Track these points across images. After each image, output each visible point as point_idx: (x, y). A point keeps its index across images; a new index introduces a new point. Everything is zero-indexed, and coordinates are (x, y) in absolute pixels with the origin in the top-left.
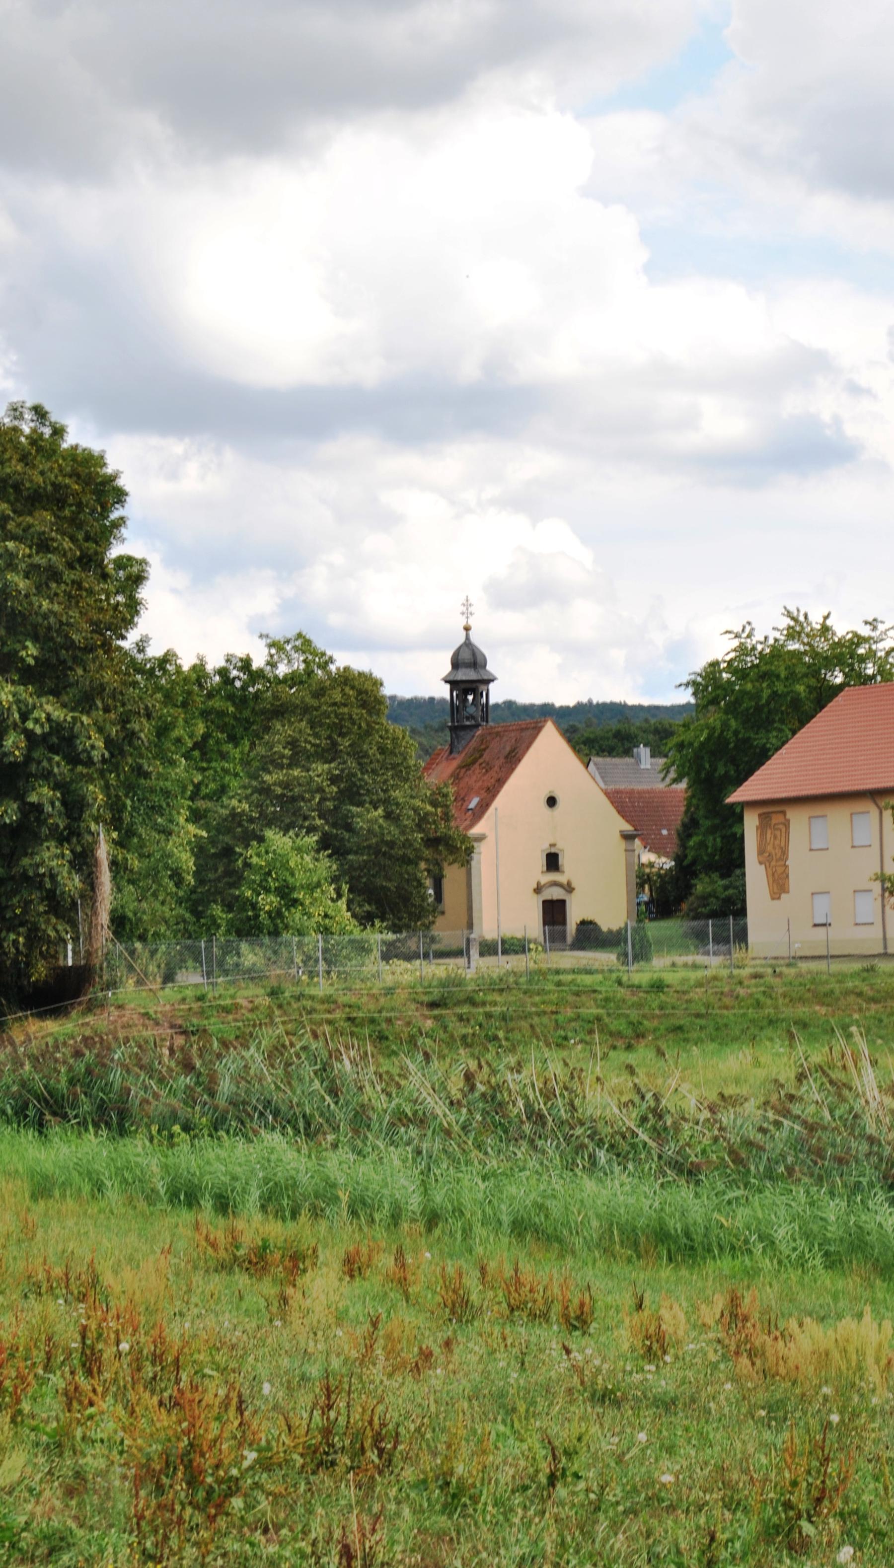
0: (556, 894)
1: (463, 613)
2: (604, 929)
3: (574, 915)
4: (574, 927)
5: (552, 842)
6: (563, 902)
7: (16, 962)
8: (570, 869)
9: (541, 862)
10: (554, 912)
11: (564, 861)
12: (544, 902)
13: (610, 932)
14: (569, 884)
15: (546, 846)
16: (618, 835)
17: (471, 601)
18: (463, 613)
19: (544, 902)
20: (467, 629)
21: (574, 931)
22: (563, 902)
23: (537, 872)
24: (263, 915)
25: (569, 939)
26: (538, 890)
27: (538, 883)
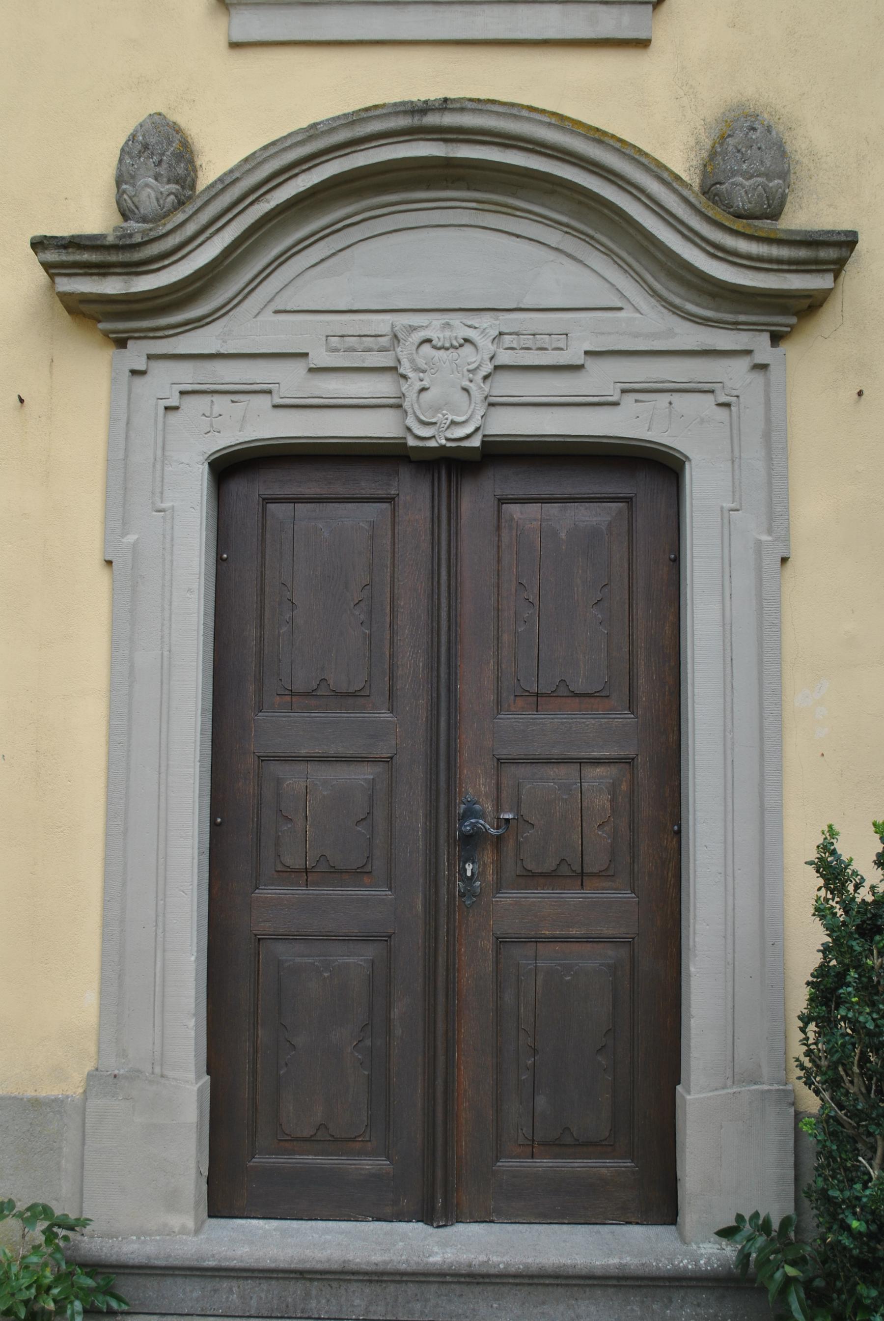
0: (444, 334)
14: (746, 178)
27: (159, 150)
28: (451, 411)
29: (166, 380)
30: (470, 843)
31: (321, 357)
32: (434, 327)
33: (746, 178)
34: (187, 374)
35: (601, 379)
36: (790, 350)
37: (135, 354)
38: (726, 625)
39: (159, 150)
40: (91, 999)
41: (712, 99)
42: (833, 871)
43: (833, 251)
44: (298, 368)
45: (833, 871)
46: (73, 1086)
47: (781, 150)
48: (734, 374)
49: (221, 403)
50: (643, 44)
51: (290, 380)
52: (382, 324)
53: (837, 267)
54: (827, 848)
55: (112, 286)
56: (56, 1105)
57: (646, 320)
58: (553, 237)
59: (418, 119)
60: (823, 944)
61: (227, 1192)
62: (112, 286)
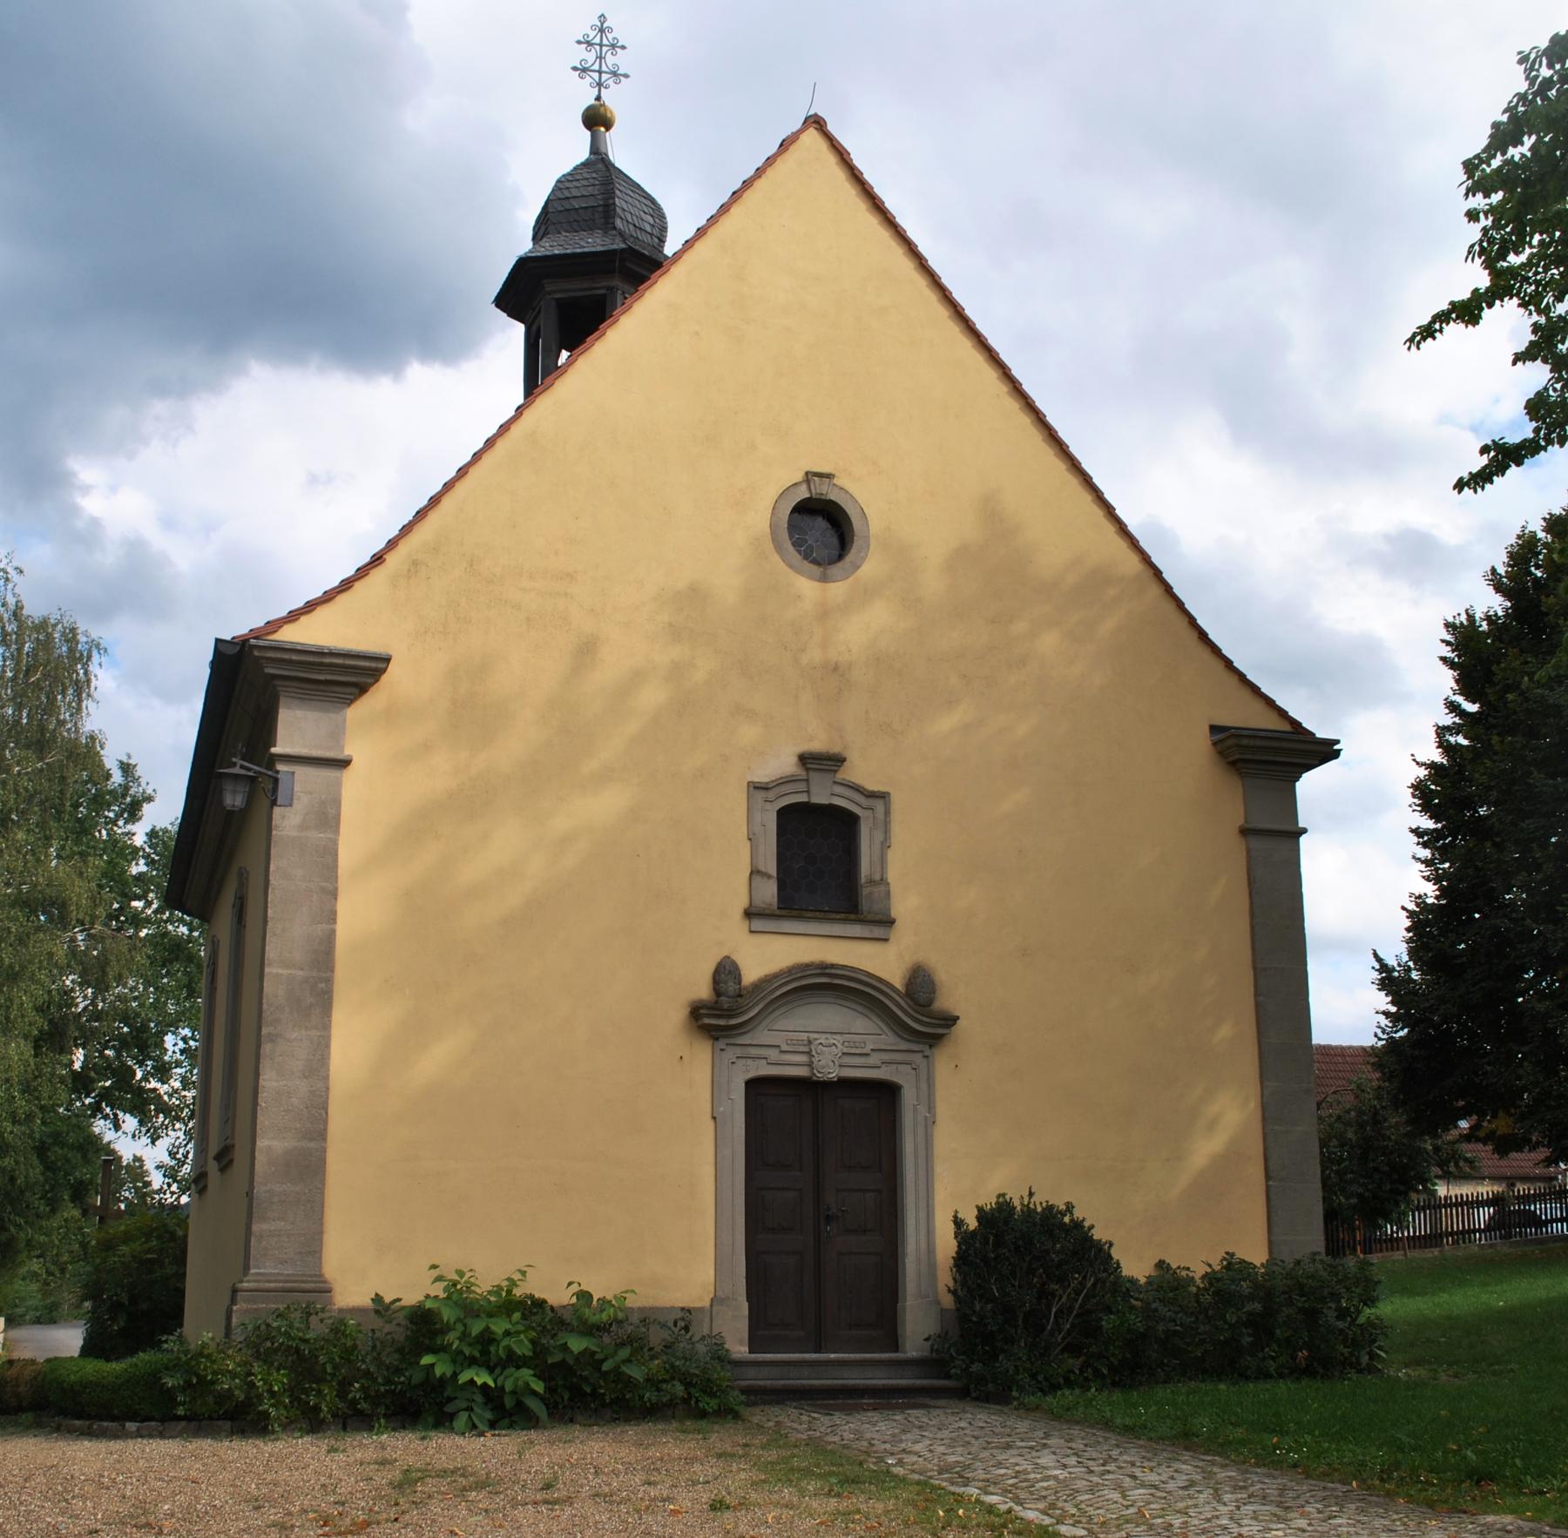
0: (832, 1043)
1: (583, 70)
2: (1135, 1265)
3: (960, 1171)
4: (946, 1244)
5: (818, 743)
6: (885, 1094)
7: (161, 1342)
8: (930, 905)
9: (732, 854)
10: (818, 1153)
11: (907, 862)
12: (757, 1088)
13: (1168, 1280)
14: (920, 985)
15: (782, 763)
16: (1202, 742)
17: (620, 30)
18: (583, 70)
19: (757, 1088)
20: (596, 119)
21: (945, 1278)
22: (885, 1094)
23: (717, 915)
24: (157, 1180)
25: (922, 1313)
26: (722, 1013)
27: (726, 972)
28: (829, 1068)
29: (731, 1053)
30: (828, 1219)
31: (785, 1048)
32: (822, 1039)
33: (920, 985)
34: (739, 1051)
35: (875, 1059)
36: (936, 1051)
37: (721, 1044)
38: (916, 1147)
39: (726, 972)
40: (712, 1272)
41: (909, 959)
42: (958, 1223)
43: (950, 1021)
44: (776, 1051)
45: (958, 1223)
46: (707, 1303)
47: (932, 983)
48: (918, 1058)
49: (749, 1062)
50: (886, 940)
51: (773, 1054)
52: (804, 1036)
53: (949, 1026)
54: (955, 1217)
55: (722, 1022)
56: (701, 1309)
57: (889, 1039)
58: (860, 1009)
59: (824, 968)
60: (1485, 450)
61: (756, 1341)
62: (722, 1022)
